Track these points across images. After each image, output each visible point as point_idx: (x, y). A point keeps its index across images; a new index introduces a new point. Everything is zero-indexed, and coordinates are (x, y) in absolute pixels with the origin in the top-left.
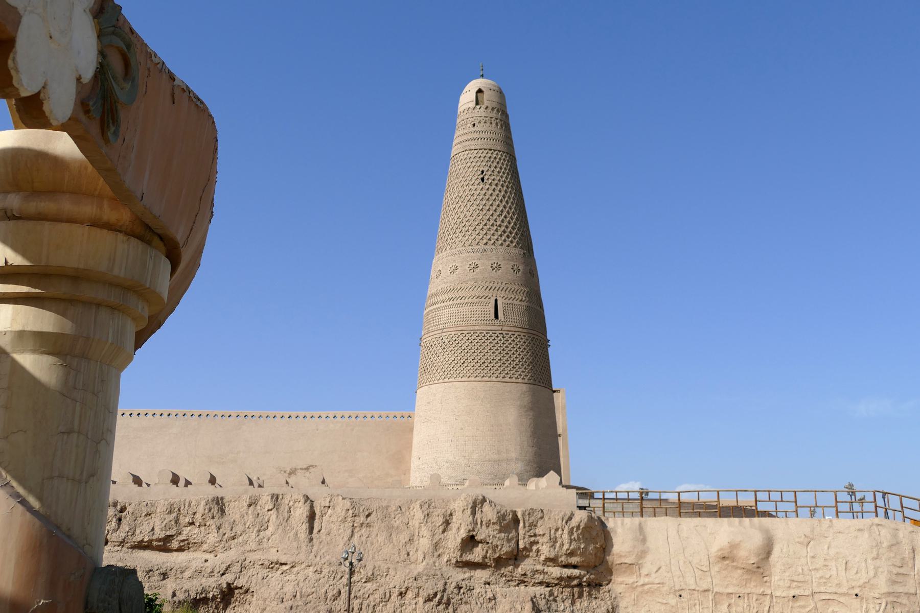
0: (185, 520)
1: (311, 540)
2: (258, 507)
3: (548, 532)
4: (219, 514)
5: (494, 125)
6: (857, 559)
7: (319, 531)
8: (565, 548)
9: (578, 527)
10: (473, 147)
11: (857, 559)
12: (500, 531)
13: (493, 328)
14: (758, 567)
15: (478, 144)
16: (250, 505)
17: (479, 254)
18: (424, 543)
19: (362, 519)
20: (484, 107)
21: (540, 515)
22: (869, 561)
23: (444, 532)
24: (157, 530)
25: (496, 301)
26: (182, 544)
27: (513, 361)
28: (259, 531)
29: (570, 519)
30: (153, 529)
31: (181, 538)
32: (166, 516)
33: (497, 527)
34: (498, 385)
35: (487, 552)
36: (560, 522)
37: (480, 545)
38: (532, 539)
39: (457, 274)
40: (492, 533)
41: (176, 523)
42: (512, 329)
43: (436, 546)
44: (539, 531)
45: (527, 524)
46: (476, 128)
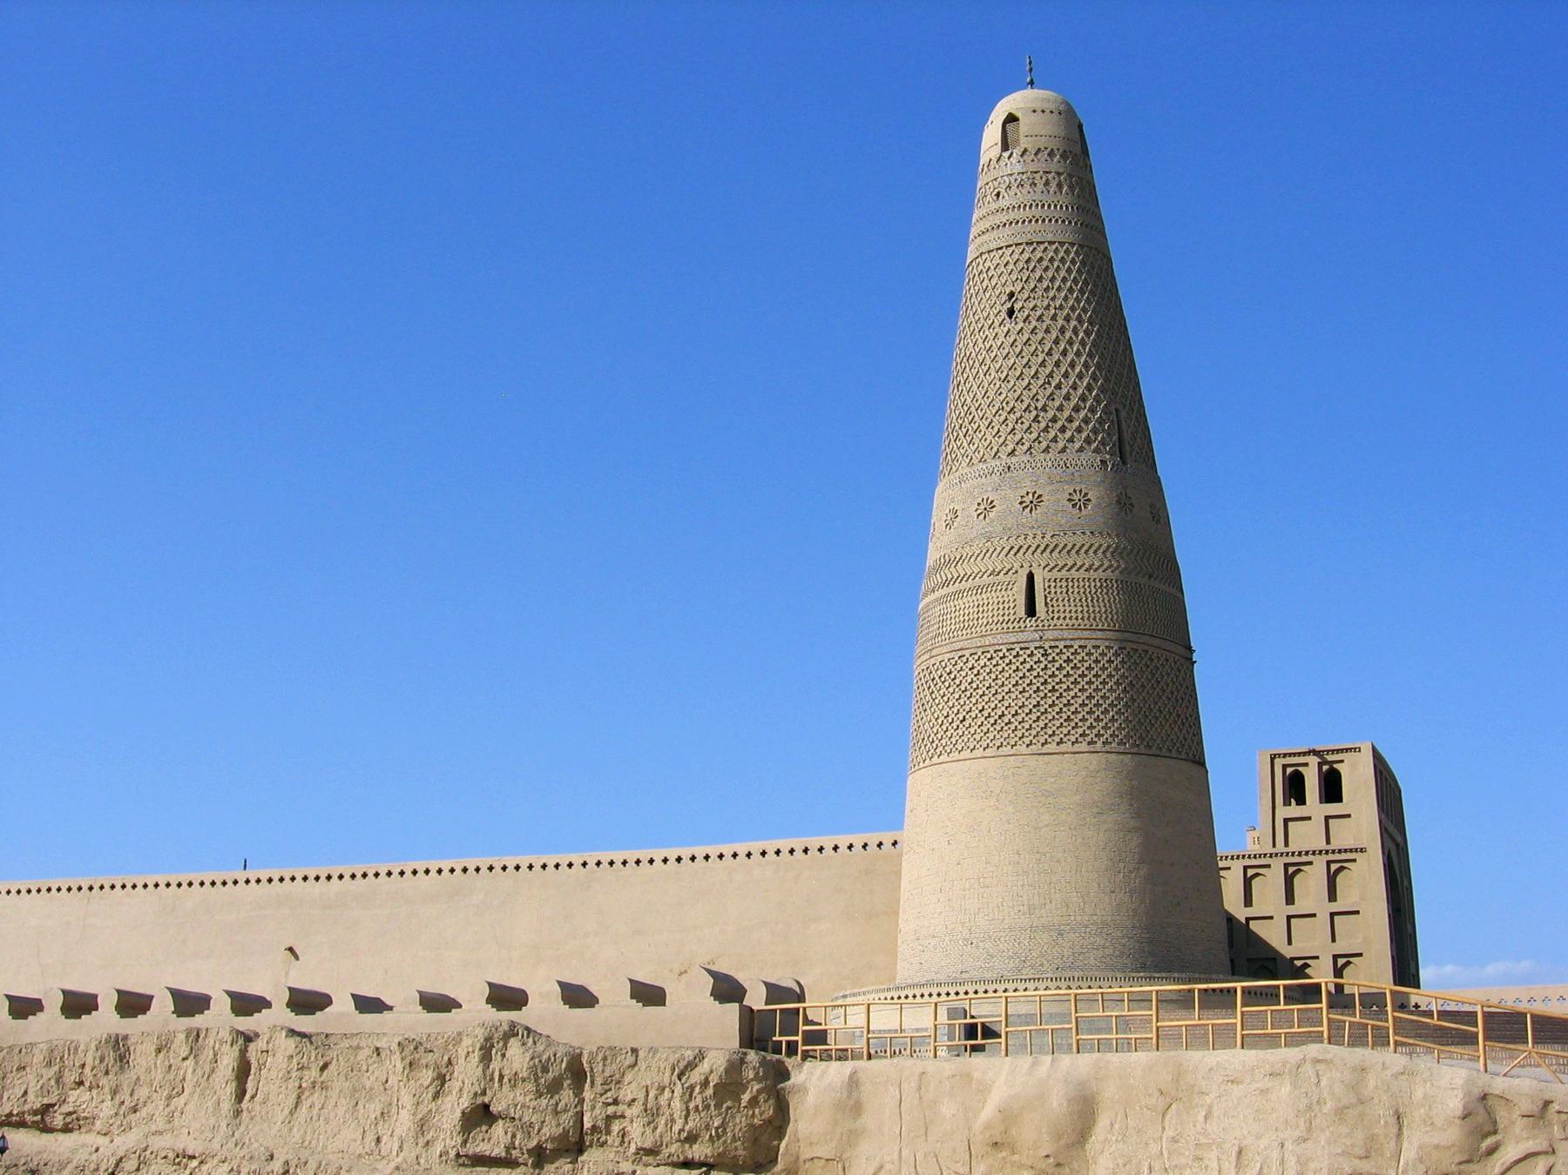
0: (70, 1077)
1: (238, 1113)
2: (171, 1054)
3: (641, 1096)
4: (117, 1068)
5: (1040, 187)
6: (1263, 1143)
7: (253, 1097)
8: (676, 1128)
9: (705, 1084)
10: (993, 246)
11: (1263, 1143)
12: (539, 1095)
13: (1021, 637)
14: (1058, 1165)
15: (1030, 232)
16: (159, 1051)
17: (996, 478)
18: (404, 1121)
19: (314, 1073)
20: (1017, 152)
21: (630, 1059)
22: (1289, 1145)
23: (436, 1096)
24: (31, 1097)
25: (1031, 577)
26: (68, 1119)
27: (1068, 704)
28: (170, 1097)
29: (691, 1066)
30: (26, 1093)
31: (66, 1108)
32: (44, 1071)
33: (531, 1086)
34: (1032, 761)
35: (514, 1136)
36: (668, 1074)
37: (501, 1122)
38: (611, 1110)
39: (986, 513)
40: (520, 1099)
41: (57, 1081)
42: (1066, 634)
43: (422, 1125)
44: (626, 1093)
45: (599, 1081)
46: (1003, 203)
